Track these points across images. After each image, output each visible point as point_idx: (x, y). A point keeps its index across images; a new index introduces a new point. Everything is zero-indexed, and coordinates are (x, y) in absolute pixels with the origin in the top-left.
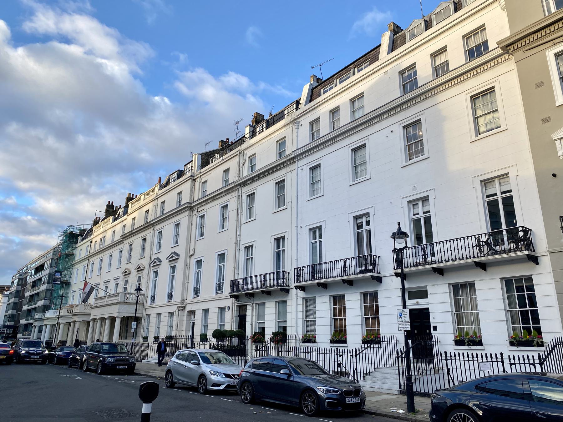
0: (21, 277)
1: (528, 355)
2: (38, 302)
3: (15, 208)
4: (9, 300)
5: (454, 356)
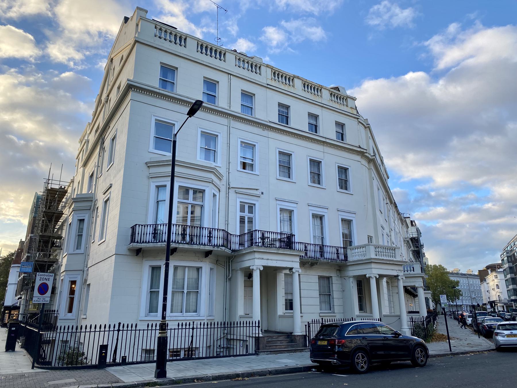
0: (508, 255)
1: (73, 325)
2: (507, 276)
3: (477, 200)
4: (505, 276)
5: (149, 326)
